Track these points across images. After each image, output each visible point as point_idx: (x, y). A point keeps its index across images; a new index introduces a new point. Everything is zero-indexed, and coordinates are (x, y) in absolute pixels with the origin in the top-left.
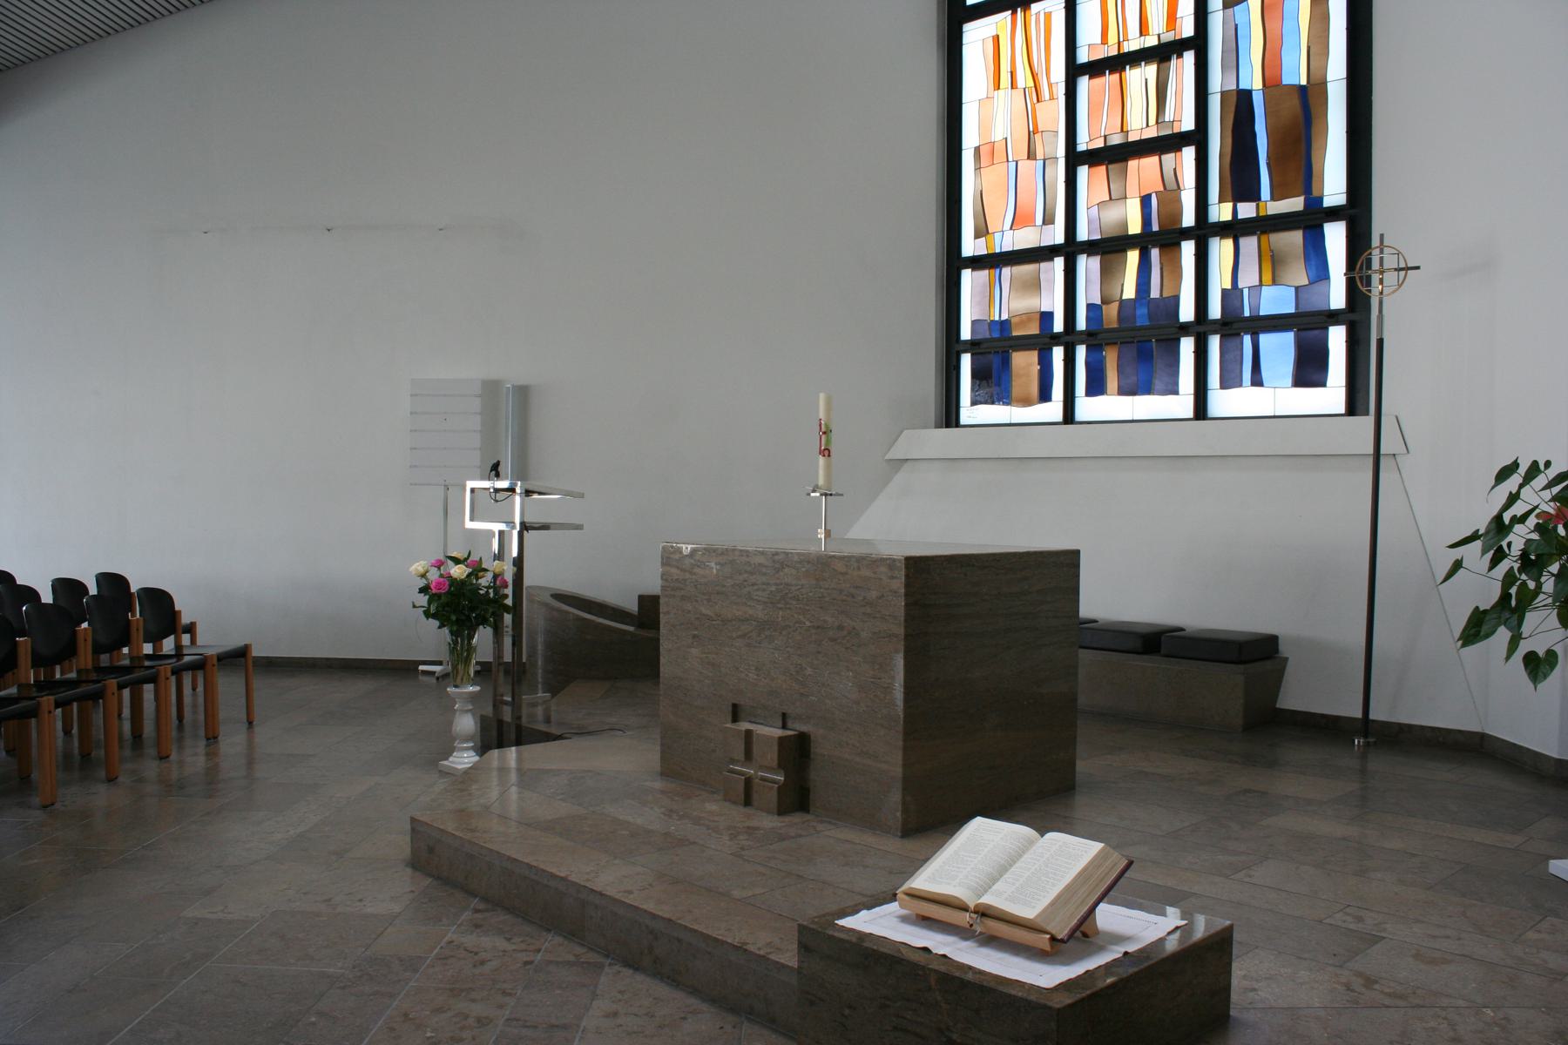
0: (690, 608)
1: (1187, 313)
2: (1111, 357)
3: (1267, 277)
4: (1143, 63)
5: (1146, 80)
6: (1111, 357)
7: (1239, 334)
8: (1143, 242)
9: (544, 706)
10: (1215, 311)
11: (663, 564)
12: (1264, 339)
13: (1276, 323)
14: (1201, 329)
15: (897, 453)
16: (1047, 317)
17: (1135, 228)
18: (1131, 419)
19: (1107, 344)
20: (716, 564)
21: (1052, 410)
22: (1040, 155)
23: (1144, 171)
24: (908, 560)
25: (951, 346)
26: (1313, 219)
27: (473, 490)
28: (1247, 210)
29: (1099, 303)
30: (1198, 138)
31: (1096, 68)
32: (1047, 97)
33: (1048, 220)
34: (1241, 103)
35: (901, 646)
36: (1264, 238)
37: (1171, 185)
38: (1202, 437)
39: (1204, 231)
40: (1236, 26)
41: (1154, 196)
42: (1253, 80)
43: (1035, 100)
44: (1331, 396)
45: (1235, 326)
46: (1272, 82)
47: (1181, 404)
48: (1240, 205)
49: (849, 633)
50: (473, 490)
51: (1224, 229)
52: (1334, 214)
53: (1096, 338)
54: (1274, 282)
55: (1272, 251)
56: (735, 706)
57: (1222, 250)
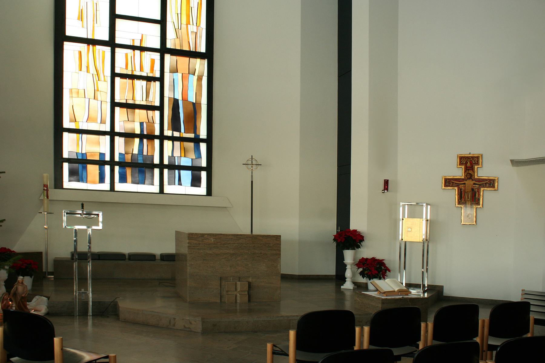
0: (202, 252)
1: (157, 161)
3: (183, 154)
4: (127, 79)
5: (142, 86)
8: (141, 136)
9: (11, 305)
16: (102, 155)
17: (138, 131)
18: (137, 191)
20: (213, 239)
22: (99, 99)
23: (140, 114)
26: (197, 141)
27: (98, 215)
30: (161, 109)
32: (103, 80)
33: (103, 122)
37: (151, 120)
39: (162, 138)
40: (174, 79)
41: (145, 123)
42: (179, 96)
43: (98, 80)
44: (202, 190)
46: (185, 100)
47: (155, 189)
49: (264, 254)
50: (98, 215)
51: (168, 138)
53: (123, 164)
55: (184, 147)
57: (168, 144)
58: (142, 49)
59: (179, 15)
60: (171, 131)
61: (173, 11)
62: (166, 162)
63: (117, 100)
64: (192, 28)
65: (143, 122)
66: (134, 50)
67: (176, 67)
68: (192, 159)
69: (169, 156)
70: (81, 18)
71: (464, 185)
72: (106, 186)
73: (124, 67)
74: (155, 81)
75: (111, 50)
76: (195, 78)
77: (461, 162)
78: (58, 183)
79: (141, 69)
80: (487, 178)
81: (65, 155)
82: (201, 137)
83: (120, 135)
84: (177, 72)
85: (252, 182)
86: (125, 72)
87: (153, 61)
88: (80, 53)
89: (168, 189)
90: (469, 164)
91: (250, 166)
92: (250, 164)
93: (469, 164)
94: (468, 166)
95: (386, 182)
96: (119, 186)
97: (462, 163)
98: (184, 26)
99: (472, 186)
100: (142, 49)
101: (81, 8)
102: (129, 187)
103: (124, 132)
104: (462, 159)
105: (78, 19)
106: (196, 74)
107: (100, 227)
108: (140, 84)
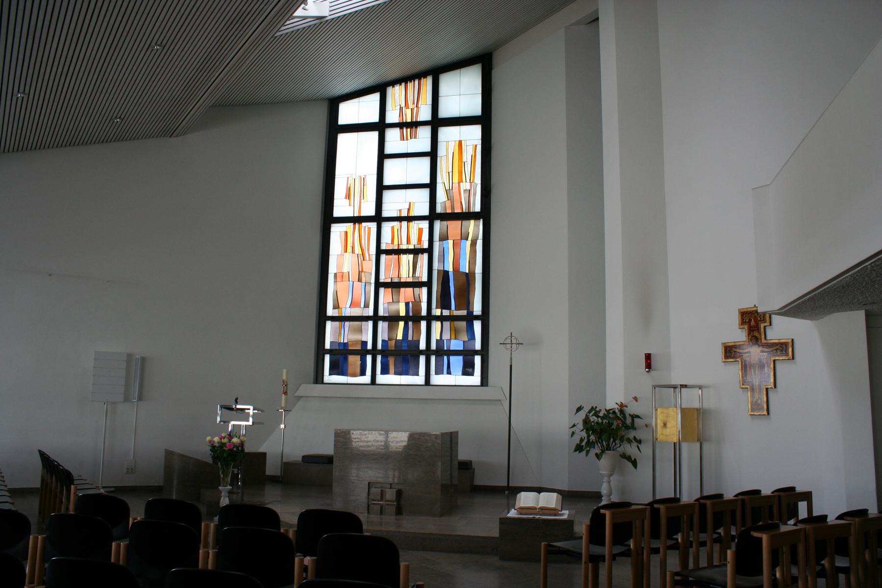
1: (423, 346)
3: (453, 336)
8: (406, 319)
22: (363, 280)
26: (470, 318)
30: (428, 284)
32: (368, 259)
33: (366, 306)
39: (430, 318)
41: (410, 303)
42: (450, 268)
43: (362, 260)
44: (475, 379)
46: (456, 269)
47: (420, 379)
51: (437, 318)
57: (436, 326)
58: (410, 219)
59: (451, 174)
60: (440, 310)
61: (444, 170)
62: (433, 346)
63: (382, 279)
64: (465, 186)
65: (409, 302)
66: (401, 222)
67: (446, 232)
68: (464, 342)
69: (437, 340)
70: (348, 196)
71: (749, 354)
72: (366, 379)
73: (390, 242)
74: (422, 254)
75: (429, 223)
76: (469, 243)
77: (744, 319)
78: (318, 378)
79: (408, 242)
80: (777, 341)
81: (328, 346)
82: (475, 313)
83: (384, 319)
84: (448, 239)
85: (511, 366)
86: (390, 247)
87: (421, 231)
88: (346, 233)
89: (381, 379)
90: (753, 323)
91: (508, 346)
92: (509, 344)
93: (753, 323)
94: (752, 324)
95: (648, 357)
96: (436, 379)
97: (744, 321)
98: (456, 185)
99: (759, 354)
100: (410, 219)
101: (349, 186)
102: (392, 379)
103: (388, 315)
104: (744, 316)
105: (346, 198)
106: (470, 238)
107: (250, 423)
108: (406, 259)
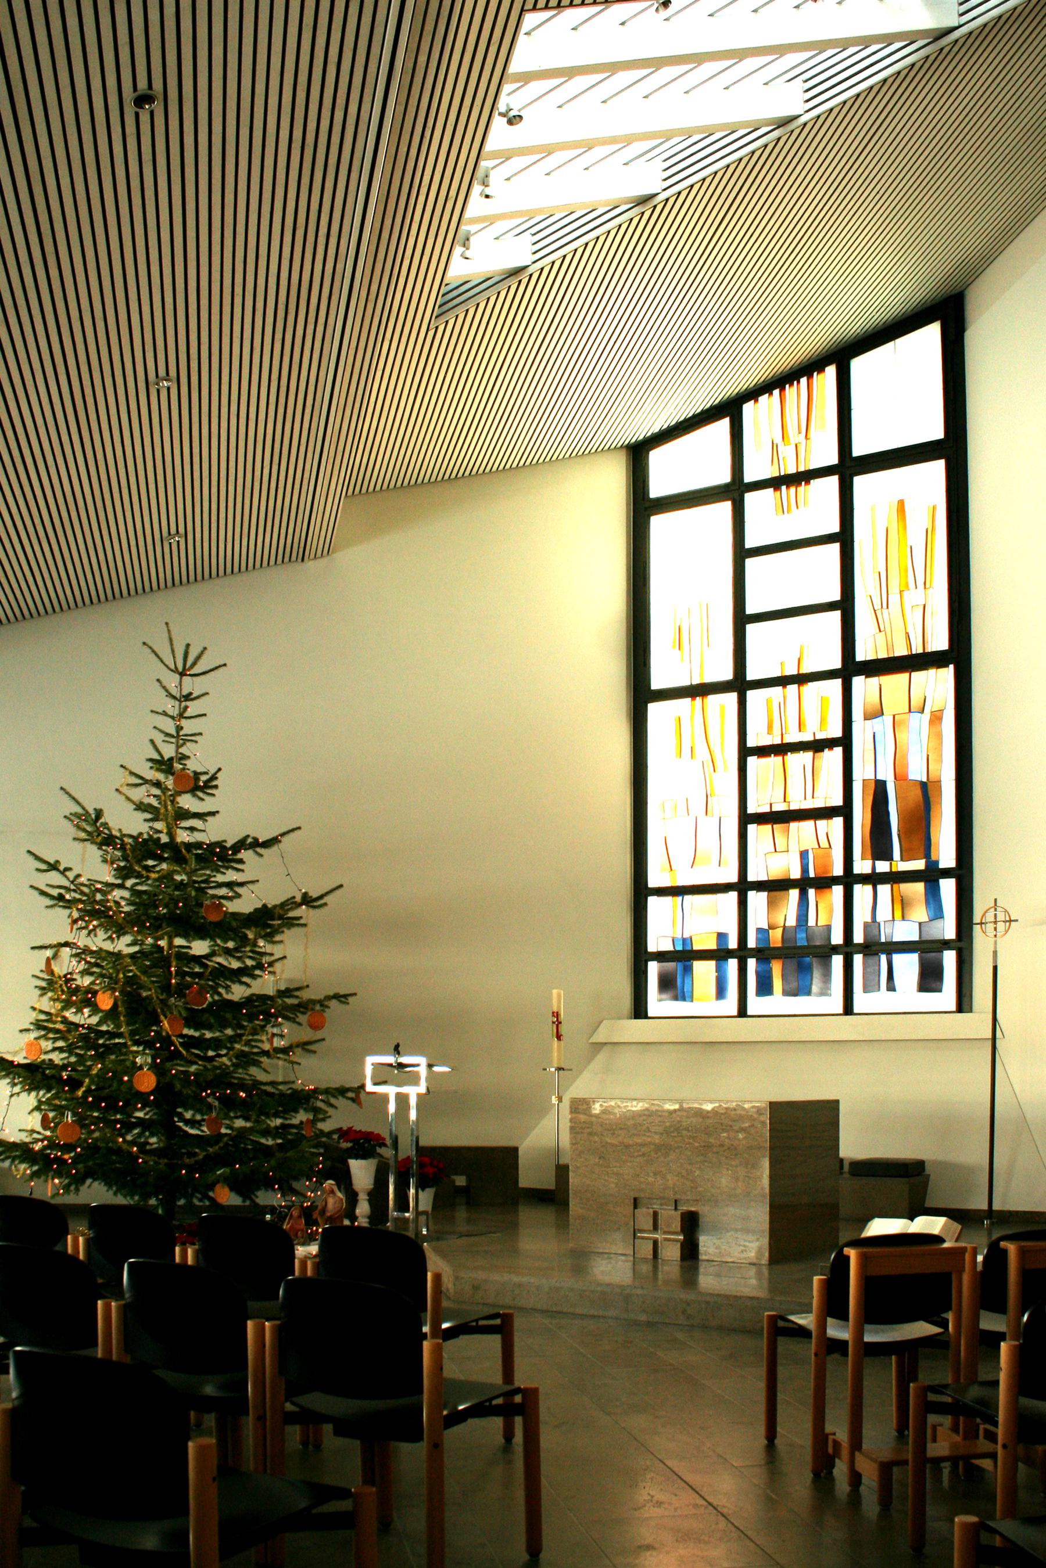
2: (776, 968)
3: (898, 914)
6: (776, 968)
7: (877, 954)
10: (858, 938)
11: (571, 1112)
12: (897, 958)
13: (905, 947)
14: (848, 950)
15: (600, 1036)
16: (722, 937)
17: (796, 874)
19: (773, 958)
21: (730, 1004)
23: (803, 832)
24: (773, 1105)
25: (640, 956)
26: (931, 876)
28: (882, 867)
29: (767, 928)
30: (845, 811)
31: (763, 751)
34: (880, 789)
35: (768, 1153)
36: (895, 886)
38: (847, 1028)
39: (849, 880)
42: (886, 774)
45: (874, 948)
46: (900, 777)
48: (877, 863)
51: (864, 879)
52: (947, 873)
54: (903, 918)
56: (635, 1199)
57: (862, 893)
